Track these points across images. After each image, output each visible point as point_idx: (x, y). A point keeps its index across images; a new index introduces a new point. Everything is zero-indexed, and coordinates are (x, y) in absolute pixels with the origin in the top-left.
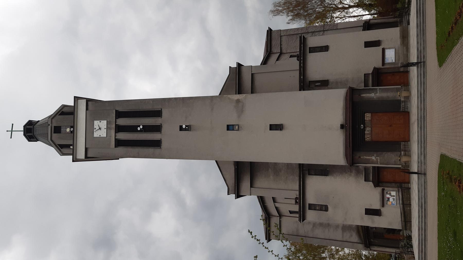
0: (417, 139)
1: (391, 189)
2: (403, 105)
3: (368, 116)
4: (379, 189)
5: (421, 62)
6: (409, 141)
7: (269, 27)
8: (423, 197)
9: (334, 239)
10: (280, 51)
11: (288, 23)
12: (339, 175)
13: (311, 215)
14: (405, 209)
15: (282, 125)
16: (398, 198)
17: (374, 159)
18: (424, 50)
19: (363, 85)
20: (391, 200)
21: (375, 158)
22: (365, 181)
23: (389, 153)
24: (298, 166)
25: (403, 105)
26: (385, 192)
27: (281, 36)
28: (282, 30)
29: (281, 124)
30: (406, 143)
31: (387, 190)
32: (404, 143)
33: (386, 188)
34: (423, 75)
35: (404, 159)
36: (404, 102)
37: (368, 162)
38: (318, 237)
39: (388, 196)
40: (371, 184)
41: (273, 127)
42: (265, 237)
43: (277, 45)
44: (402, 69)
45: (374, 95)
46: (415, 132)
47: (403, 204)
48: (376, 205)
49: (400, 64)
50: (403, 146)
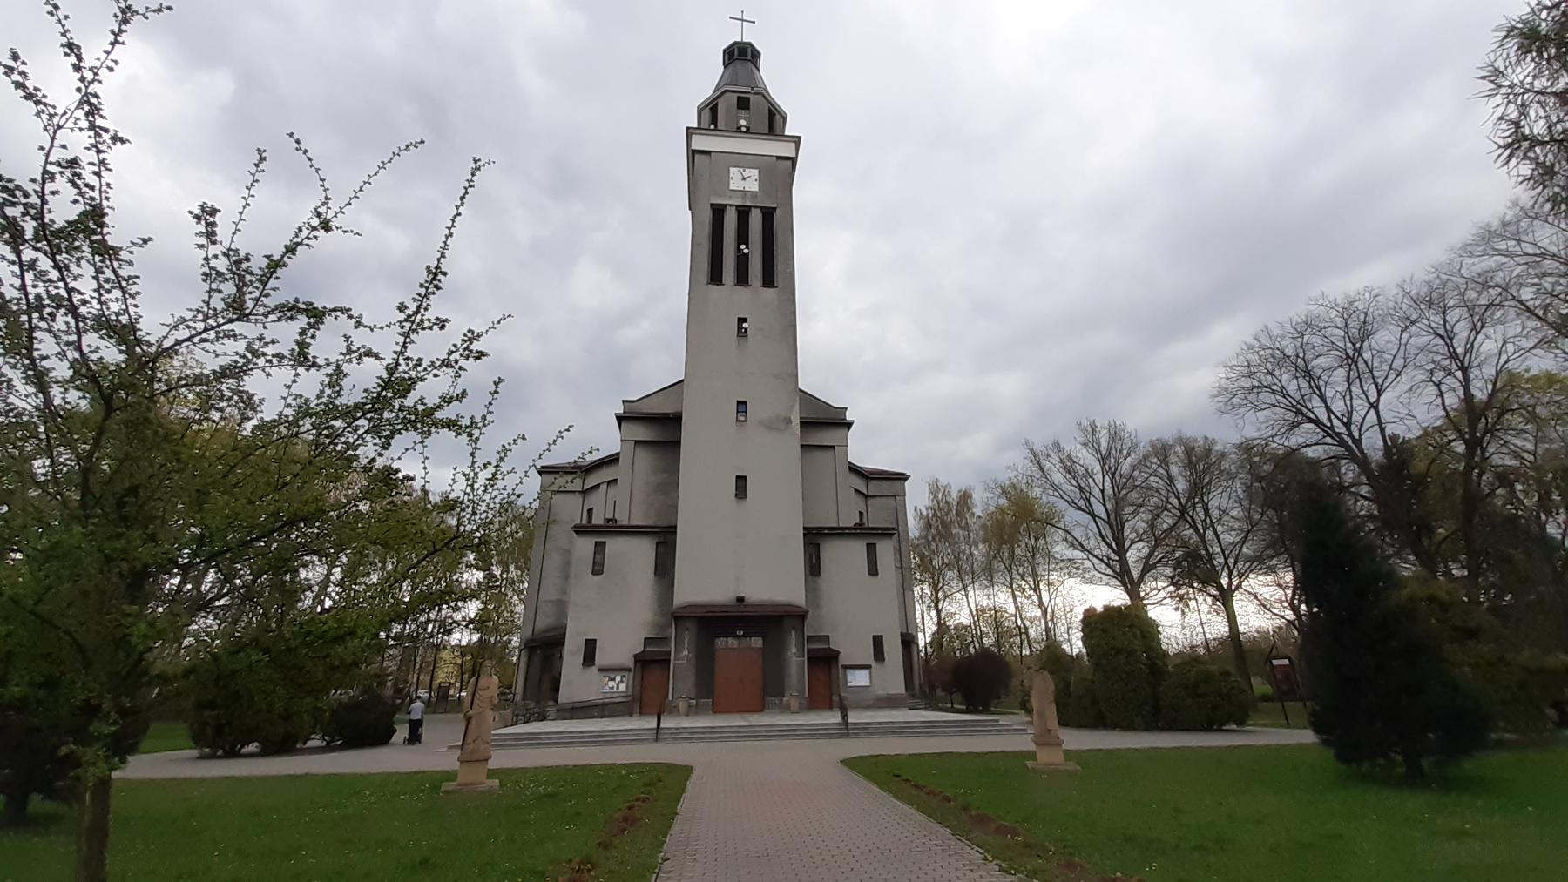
1: (631, 682)
3: (757, 642)
4: (630, 663)
10: (870, 494)
11: (916, 509)
13: (586, 545)
16: (615, 695)
20: (611, 684)
22: (646, 639)
24: (673, 524)
26: (626, 674)
33: (632, 674)
35: (683, 705)
39: (618, 678)
41: (741, 481)
44: (835, 698)
48: (601, 658)
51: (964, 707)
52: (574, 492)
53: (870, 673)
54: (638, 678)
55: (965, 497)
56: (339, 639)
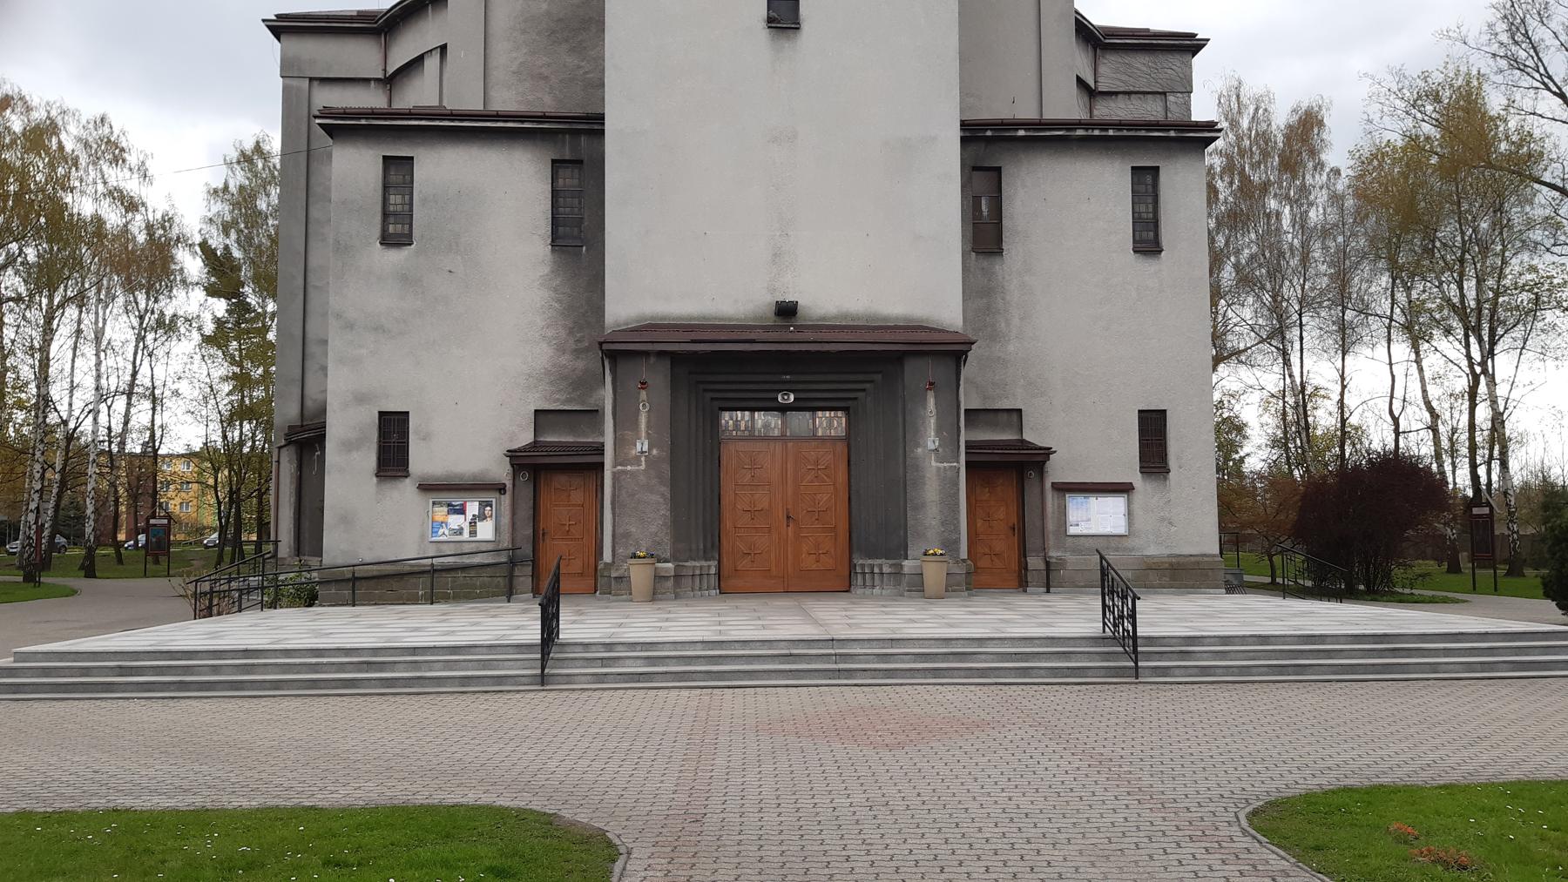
0: (730, 638)
1: (506, 520)
2: (881, 569)
3: (830, 423)
4: (501, 471)
5: (1135, 655)
6: (720, 593)
7: (1208, 40)
8: (419, 670)
9: (310, 307)
10: (1102, 88)
12: (559, 301)
14: (415, 580)
15: (798, 28)
16: (467, 548)
17: (639, 449)
18: (1196, 670)
19: (975, 404)
20: (455, 521)
21: (642, 452)
22: (536, 411)
23: (665, 511)
24: (591, 110)
25: (880, 567)
26: (492, 497)
27: (1164, 94)
28: (1190, 97)
29: (799, 23)
30: (713, 581)
31: (499, 503)
32: (713, 571)
33: (506, 500)
34: (1068, 668)
35: (639, 574)
36: (898, 574)
37: (625, 421)
38: (312, 243)
39: (473, 508)
40: (526, 437)
42: (287, 12)
43: (1124, 78)
44: (1034, 562)
45: (931, 446)
46: (764, 627)
47: (434, 571)
48: (424, 459)
49: (1059, 554)
50: (701, 567)
51: (1309, 583)
52: (366, 81)
53: (1129, 503)
54: (525, 510)
55: (1307, 126)
56: (87, 447)
